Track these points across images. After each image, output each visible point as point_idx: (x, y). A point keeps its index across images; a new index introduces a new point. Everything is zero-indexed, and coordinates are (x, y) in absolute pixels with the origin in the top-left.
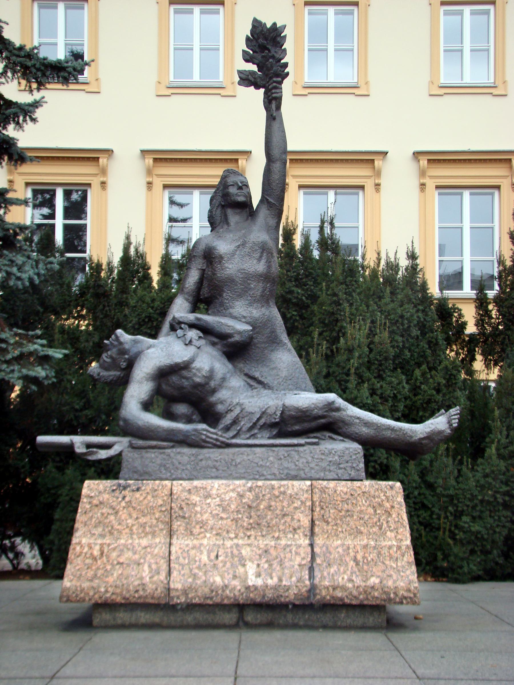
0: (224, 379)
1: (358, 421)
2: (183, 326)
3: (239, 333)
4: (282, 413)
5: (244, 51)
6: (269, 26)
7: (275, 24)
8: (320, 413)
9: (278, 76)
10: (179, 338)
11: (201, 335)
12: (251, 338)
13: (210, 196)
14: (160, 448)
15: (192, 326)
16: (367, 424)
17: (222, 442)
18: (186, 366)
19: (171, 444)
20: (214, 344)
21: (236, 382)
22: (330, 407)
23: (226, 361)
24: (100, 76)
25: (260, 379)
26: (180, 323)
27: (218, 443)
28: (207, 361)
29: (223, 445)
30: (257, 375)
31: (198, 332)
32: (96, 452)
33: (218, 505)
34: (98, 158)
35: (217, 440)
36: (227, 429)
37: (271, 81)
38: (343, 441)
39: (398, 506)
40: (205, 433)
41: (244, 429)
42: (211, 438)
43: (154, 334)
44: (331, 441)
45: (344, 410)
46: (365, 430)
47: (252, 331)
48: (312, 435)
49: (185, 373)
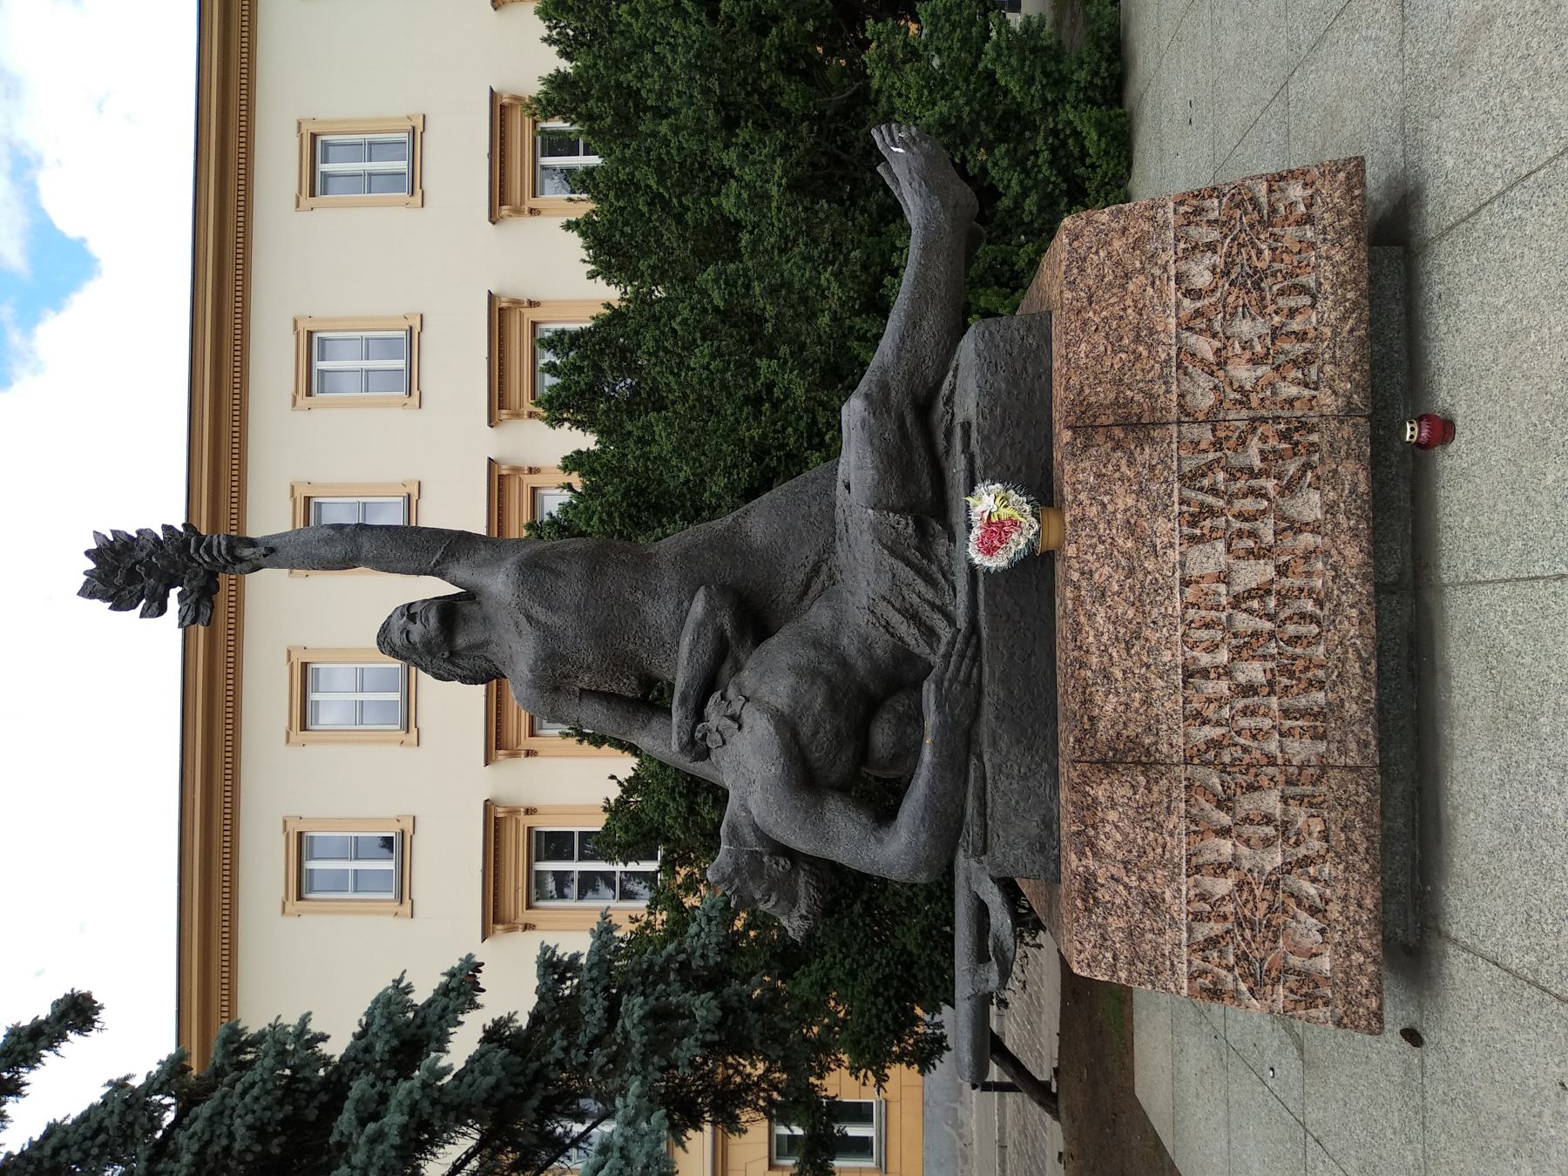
0: (817, 644)
2: (698, 735)
3: (711, 611)
5: (142, 616)
6: (91, 565)
7: (88, 553)
8: (892, 426)
9: (187, 544)
10: (724, 742)
11: (717, 695)
12: (723, 589)
13: (426, 679)
14: (982, 803)
15: (699, 715)
16: (913, 322)
17: (967, 642)
18: (786, 726)
19: (974, 761)
20: (738, 669)
21: (819, 616)
22: (879, 403)
23: (774, 641)
24: (394, 815)
25: (808, 569)
26: (692, 741)
27: (969, 653)
28: (772, 679)
29: (974, 641)
30: (800, 576)
31: (711, 702)
32: (997, 938)
33: (1128, 650)
35: (962, 656)
36: (930, 634)
37: (196, 556)
38: (956, 369)
39: (1122, 218)
40: (946, 684)
41: (929, 594)
42: (958, 670)
43: (720, 797)
44: (957, 399)
46: (932, 323)
47: (708, 587)
48: (941, 443)
49: (805, 730)
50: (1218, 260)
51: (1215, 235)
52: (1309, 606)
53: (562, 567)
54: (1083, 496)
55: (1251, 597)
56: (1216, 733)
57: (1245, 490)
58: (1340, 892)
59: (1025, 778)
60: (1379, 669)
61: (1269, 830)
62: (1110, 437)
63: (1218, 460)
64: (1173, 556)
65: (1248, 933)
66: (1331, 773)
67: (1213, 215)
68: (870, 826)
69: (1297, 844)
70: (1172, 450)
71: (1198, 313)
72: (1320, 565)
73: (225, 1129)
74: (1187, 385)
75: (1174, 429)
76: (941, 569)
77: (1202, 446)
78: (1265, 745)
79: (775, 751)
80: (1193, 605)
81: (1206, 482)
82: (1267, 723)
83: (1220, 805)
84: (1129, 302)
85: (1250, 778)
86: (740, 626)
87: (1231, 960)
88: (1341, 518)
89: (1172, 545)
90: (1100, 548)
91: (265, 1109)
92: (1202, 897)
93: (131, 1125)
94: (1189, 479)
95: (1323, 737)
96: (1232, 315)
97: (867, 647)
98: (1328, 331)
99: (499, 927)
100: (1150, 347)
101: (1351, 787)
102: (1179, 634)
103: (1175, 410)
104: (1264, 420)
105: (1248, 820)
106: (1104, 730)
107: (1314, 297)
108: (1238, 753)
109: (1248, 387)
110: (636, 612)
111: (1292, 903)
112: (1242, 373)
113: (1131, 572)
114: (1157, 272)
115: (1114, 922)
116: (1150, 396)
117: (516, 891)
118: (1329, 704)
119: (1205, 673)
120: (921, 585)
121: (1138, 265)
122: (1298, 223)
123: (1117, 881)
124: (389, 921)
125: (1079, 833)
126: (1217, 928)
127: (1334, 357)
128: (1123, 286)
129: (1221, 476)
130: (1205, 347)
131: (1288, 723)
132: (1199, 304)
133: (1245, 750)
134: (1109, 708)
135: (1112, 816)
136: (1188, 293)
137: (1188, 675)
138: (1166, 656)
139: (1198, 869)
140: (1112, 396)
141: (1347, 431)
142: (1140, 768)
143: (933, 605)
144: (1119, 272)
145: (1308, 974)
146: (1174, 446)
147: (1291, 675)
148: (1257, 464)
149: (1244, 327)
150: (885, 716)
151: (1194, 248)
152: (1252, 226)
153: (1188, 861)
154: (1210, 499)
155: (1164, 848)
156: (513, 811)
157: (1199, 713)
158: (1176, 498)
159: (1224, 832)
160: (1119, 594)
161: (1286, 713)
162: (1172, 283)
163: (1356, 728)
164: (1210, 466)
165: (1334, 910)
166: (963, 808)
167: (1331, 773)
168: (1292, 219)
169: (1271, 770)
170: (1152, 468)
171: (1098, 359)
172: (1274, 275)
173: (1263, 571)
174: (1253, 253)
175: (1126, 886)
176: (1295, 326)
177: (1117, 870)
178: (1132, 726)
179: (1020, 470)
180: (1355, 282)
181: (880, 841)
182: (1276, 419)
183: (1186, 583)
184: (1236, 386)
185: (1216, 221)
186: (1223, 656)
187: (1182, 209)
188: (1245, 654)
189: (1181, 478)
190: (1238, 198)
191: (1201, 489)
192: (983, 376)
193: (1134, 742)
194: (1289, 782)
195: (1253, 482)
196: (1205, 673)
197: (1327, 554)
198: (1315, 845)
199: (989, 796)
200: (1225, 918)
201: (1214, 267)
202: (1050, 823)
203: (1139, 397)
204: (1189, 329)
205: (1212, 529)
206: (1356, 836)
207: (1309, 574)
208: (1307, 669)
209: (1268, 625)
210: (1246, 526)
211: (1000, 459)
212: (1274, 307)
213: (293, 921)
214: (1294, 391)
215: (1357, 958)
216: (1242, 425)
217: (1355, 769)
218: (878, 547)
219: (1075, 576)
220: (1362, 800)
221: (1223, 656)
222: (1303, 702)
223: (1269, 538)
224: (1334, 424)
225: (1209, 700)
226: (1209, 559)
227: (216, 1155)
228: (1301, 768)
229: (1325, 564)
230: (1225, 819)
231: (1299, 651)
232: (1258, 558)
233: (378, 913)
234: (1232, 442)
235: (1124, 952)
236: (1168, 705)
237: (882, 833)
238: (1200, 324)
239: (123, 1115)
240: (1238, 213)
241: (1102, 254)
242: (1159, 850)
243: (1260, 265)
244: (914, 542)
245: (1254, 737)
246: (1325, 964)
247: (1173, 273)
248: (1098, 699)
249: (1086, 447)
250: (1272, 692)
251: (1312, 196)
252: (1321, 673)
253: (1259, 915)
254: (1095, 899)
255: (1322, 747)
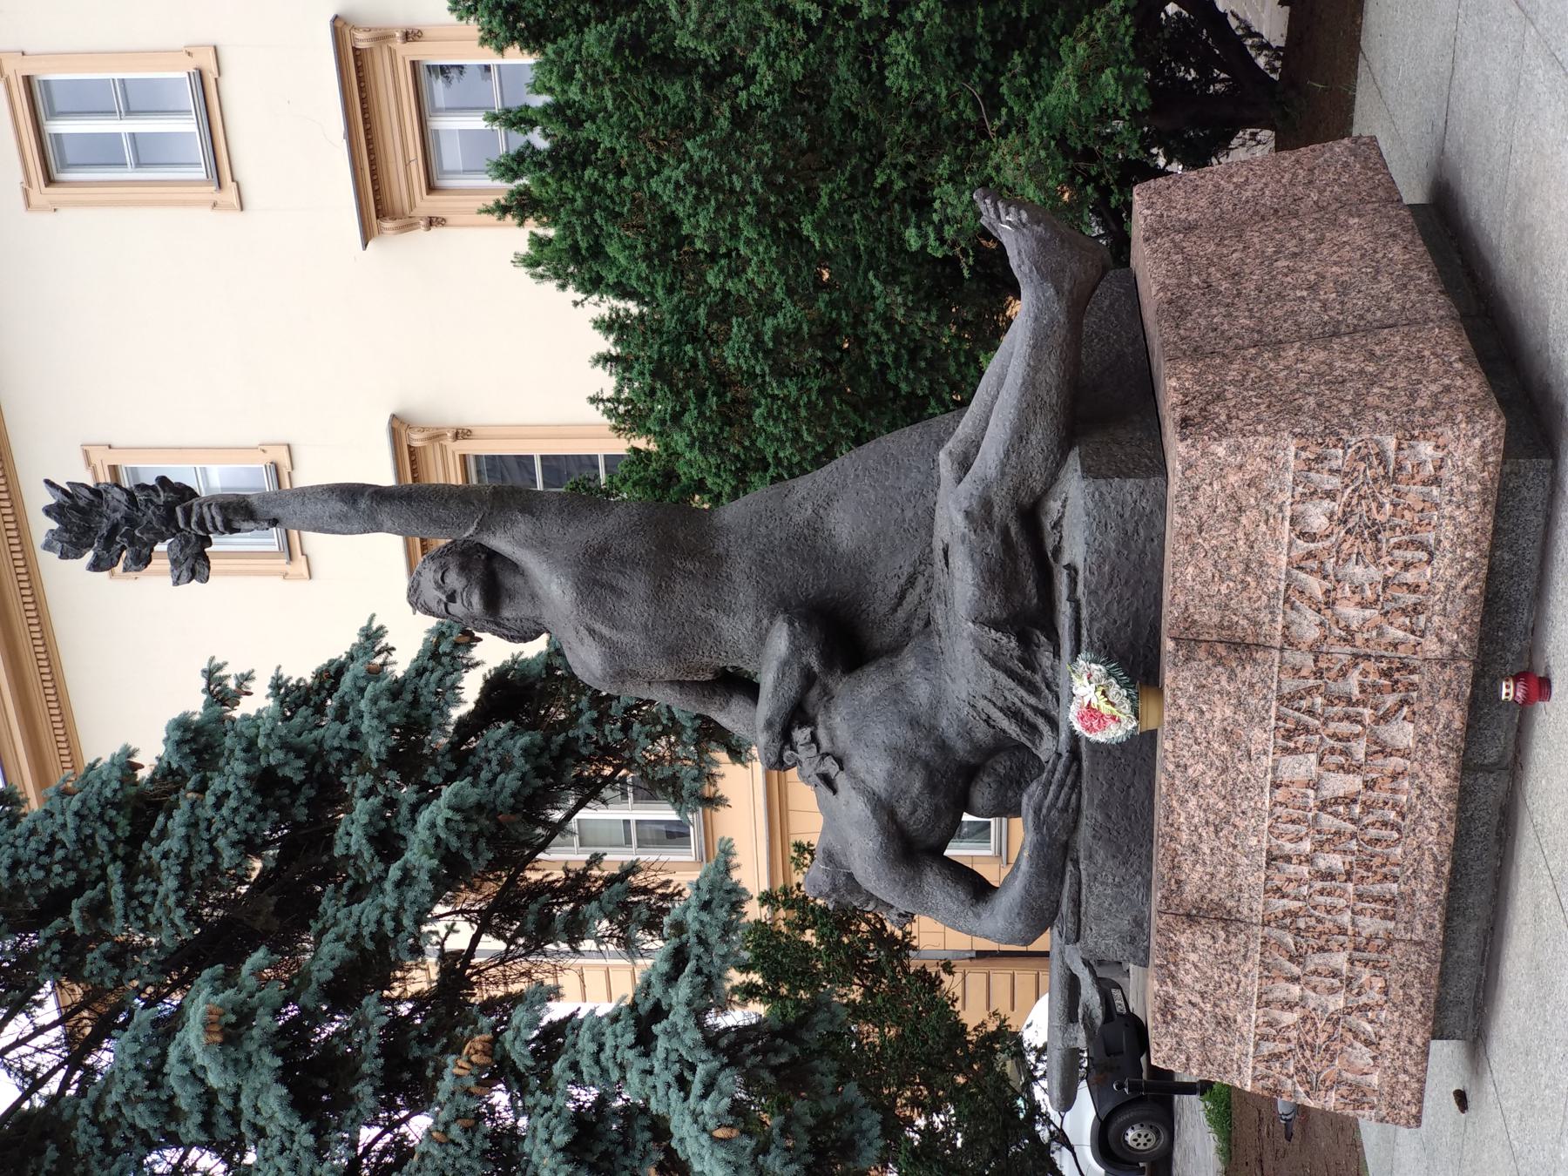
0: (914, 722)
1: (1013, 456)
3: (796, 650)
4: (995, 625)
8: (994, 540)
14: (1077, 902)
17: (1067, 771)
19: (1070, 867)
24: (180, 43)
25: (902, 581)
27: (1069, 782)
29: (1074, 768)
30: (894, 589)
32: (1087, 1007)
33: (1216, 832)
34: (355, 49)
35: (1061, 786)
40: (1044, 811)
45: (988, 487)
49: (903, 811)
50: (1337, 507)
51: (1336, 482)
52: (1392, 815)
53: (623, 583)
54: (1182, 702)
55: (1336, 803)
56: (1294, 905)
57: (1341, 714)
58: (1394, 1032)
59: (1119, 886)
60: (1451, 872)
61: (1336, 982)
62: (1210, 654)
63: (1318, 688)
64: (1267, 762)
65: (1308, 1054)
66: (1396, 945)
67: (1335, 464)
68: (967, 903)
69: (1359, 994)
70: (1268, 676)
71: (1310, 555)
72: (1406, 784)
73: (206, 846)
74: (1293, 615)
75: (1276, 654)
76: (1045, 679)
77: (1304, 673)
78: (1338, 918)
79: (873, 831)
80: (1281, 804)
81: (1304, 704)
82: (1341, 903)
83: (1291, 959)
84: (1240, 535)
85: (1322, 942)
86: (828, 662)
87: (1292, 1070)
88: (1431, 746)
89: (1265, 753)
90: (1195, 748)
91: (247, 820)
92: (1270, 1024)
93: (92, 836)
94: (1285, 699)
95: (1393, 918)
96: (1345, 561)
97: (967, 733)
98: (1441, 587)
99: (388, 224)
100: (1258, 578)
101: (1414, 958)
102: (1266, 825)
103: (1279, 638)
104: (1368, 657)
105: (1315, 972)
106: (1190, 893)
107: (1431, 554)
108: (1313, 922)
109: (1354, 627)
110: (709, 628)
111: (1350, 1035)
112: (1350, 611)
113: (1225, 770)
114: (1272, 510)
115: (1188, 1034)
116: (1256, 623)
117: (407, 165)
118: (1401, 893)
119: (1288, 859)
120: (1022, 692)
121: (1252, 501)
122: (1424, 483)
123: (1194, 1005)
124: (203, 217)
125: (1161, 966)
126: (1281, 1047)
127: (1444, 609)
128: (1236, 520)
129: (1319, 700)
130: (1315, 586)
131: (1360, 905)
132: (1312, 546)
133: (1319, 921)
134: (1196, 876)
135: (1193, 957)
136: (1302, 535)
137: (1271, 859)
138: (1253, 841)
139: (1267, 1004)
140: (1216, 619)
141: (1448, 673)
142: (1221, 924)
143: (1035, 710)
144: (1232, 506)
145: (1358, 1087)
146: (1276, 669)
147: (1369, 868)
148: (1356, 691)
149: (1358, 572)
150: (986, 779)
151: (1312, 494)
152: (1375, 480)
153: (1259, 997)
154: (1306, 718)
155: (1238, 984)
156: (383, 37)
157: (1279, 889)
158: (1273, 713)
159: (1295, 980)
160: (1211, 787)
161: (1360, 897)
162: (1287, 523)
163: (1424, 913)
164: (1309, 691)
165: (1386, 1044)
166: (1058, 903)
167: (1396, 945)
168: (1418, 478)
169: (1341, 938)
170: (1252, 686)
171: (1204, 584)
172: (1393, 529)
173: (1353, 783)
174: (1374, 506)
175: (1201, 1011)
176: (1410, 577)
177: (1196, 999)
178: (1216, 891)
179: (1127, 624)
180: (1477, 542)
181: (978, 916)
182: (1379, 658)
183: (1276, 785)
184: (1342, 624)
185: (1338, 471)
186: (1306, 846)
187: (1304, 455)
188: (1326, 847)
189: (1280, 698)
190: (1364, 451)
191: (1298, 710)
192: (1092, 534)
193: (1220, 905)
194: (1355, 949)
195: (1350, 709)
196: (1288, 859)
197: (1415, 776)
198: (1374, 996)
199: (1083, 898)
200: (1289, 1040)
201: (1332, 514)
202: (1140, 923)
203: (1244, 622)
204: (1300, 568)
205: (1306, 744)
206: (1413, 992)
207: (1394, 791)
208: (1384, 865)
209: (1351, 827)
210: (1338, 745)
211: (1107, 613)
212: (1389, 558)
213: (48, 218)
214: (1401, 634)
215: (1403, 1077)
216: (1346, 659)
217: (1421, 943)
218: (979, 657)
219: (1171, 767)
220: (1422, 967)
221: (1306, 846)
222: (1377, 889)
223: (1361, 756)
224: (1436, 668)
225: (1290, 880)
226: (1301, 767)
227: (202, 872)
228: (1369, 940)
229: (1411, 784)
230: (1296, 970)
231: (1378, 849)
232: (1347, 772)
233: (185, 203)
234: (1333, 673)
235: (1197, 1056)
236: (1251, 879)
237: (979, 909)
238: (1314, 564)
239: (78, 830)
240: (1362, 466)
241: (1216, 486)
242: (1234, 986)
243: (1379, 518)
244: (1017, 653)
245: (1328, 912)
246: (1375, 1079)
247: (1288, 513)
248: (1186, 867)
249: (1187, 660)
250: (1348, 879)
251: (1442, 460)
252: (1397, 870)
253: (1319, 1042)
254: (1173, 1016)
255: (1391, 925)
